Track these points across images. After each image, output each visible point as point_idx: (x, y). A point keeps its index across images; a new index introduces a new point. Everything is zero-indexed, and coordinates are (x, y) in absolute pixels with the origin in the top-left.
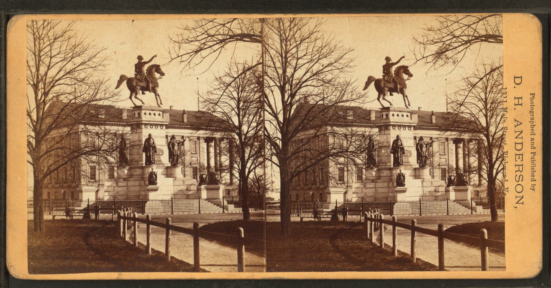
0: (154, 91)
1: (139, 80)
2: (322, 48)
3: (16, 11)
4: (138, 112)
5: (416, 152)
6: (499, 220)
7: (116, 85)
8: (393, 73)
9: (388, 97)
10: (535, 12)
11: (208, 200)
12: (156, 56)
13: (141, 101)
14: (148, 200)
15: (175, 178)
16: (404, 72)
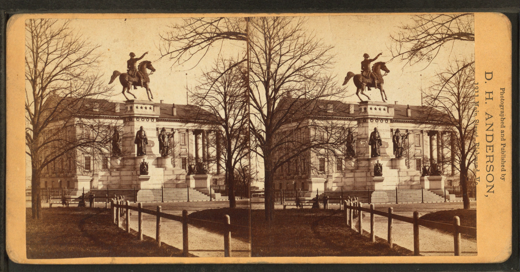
1: (132, 76)
2: (304, 45)
3: (15, 11)
4: (130, 105)
5: (392, 143)
6: (471, 207)
7: (109, 81)
8: (371, 69)
9: (366, 91)
10: (505, 12)
11: (197, 188)
12: (147, 53)
13: (133, 95)
14: (140, 189)
15: (165, 168)
16: (381, 68)
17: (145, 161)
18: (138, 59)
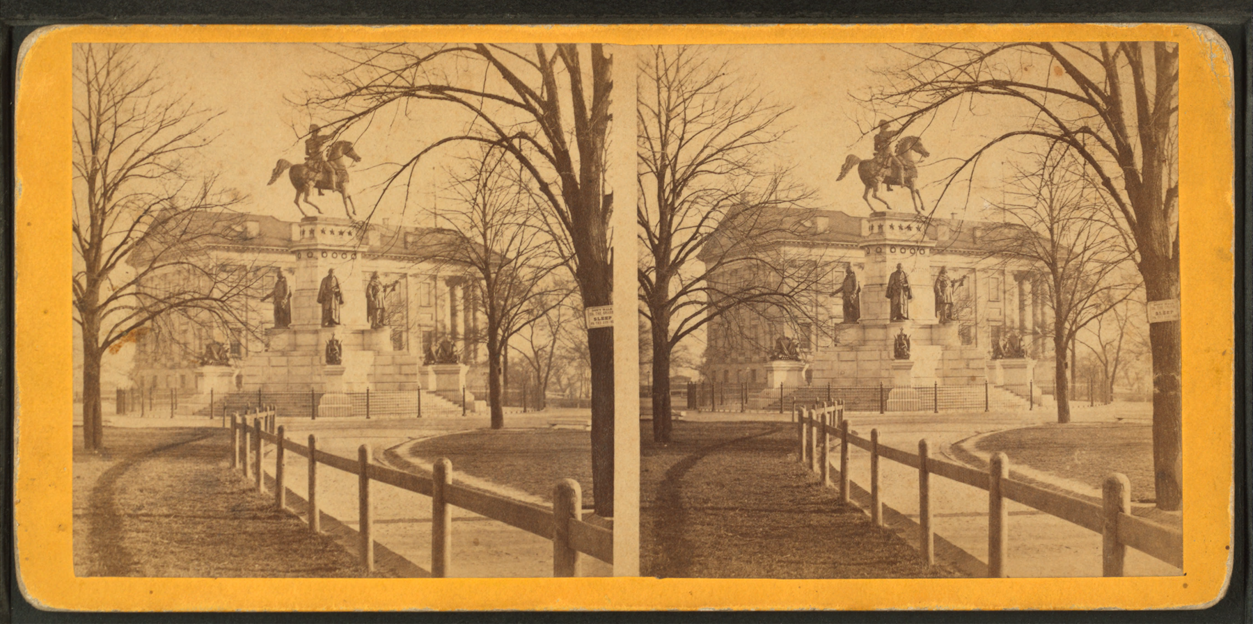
0: (340, 188)
7: (838, 175)
17: (905, 332)
18: (325, 138)
